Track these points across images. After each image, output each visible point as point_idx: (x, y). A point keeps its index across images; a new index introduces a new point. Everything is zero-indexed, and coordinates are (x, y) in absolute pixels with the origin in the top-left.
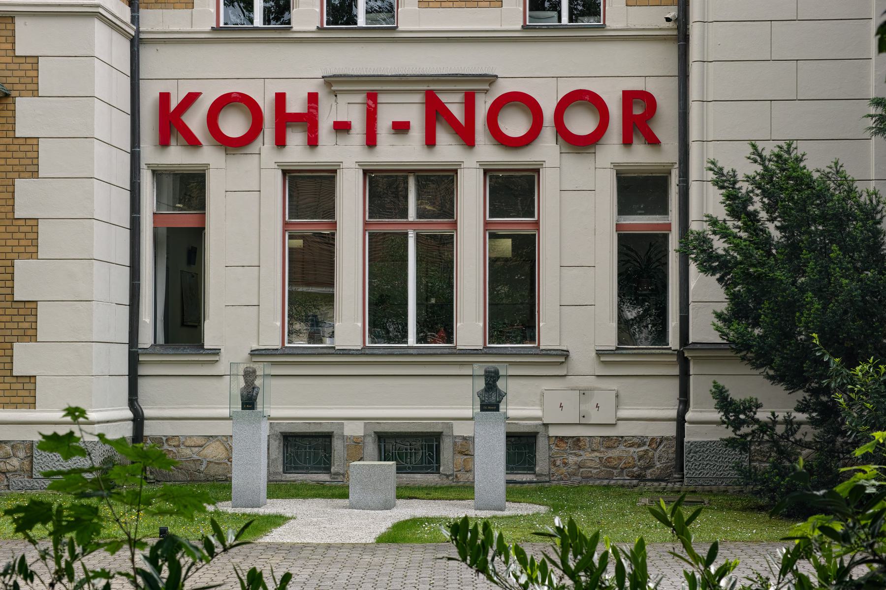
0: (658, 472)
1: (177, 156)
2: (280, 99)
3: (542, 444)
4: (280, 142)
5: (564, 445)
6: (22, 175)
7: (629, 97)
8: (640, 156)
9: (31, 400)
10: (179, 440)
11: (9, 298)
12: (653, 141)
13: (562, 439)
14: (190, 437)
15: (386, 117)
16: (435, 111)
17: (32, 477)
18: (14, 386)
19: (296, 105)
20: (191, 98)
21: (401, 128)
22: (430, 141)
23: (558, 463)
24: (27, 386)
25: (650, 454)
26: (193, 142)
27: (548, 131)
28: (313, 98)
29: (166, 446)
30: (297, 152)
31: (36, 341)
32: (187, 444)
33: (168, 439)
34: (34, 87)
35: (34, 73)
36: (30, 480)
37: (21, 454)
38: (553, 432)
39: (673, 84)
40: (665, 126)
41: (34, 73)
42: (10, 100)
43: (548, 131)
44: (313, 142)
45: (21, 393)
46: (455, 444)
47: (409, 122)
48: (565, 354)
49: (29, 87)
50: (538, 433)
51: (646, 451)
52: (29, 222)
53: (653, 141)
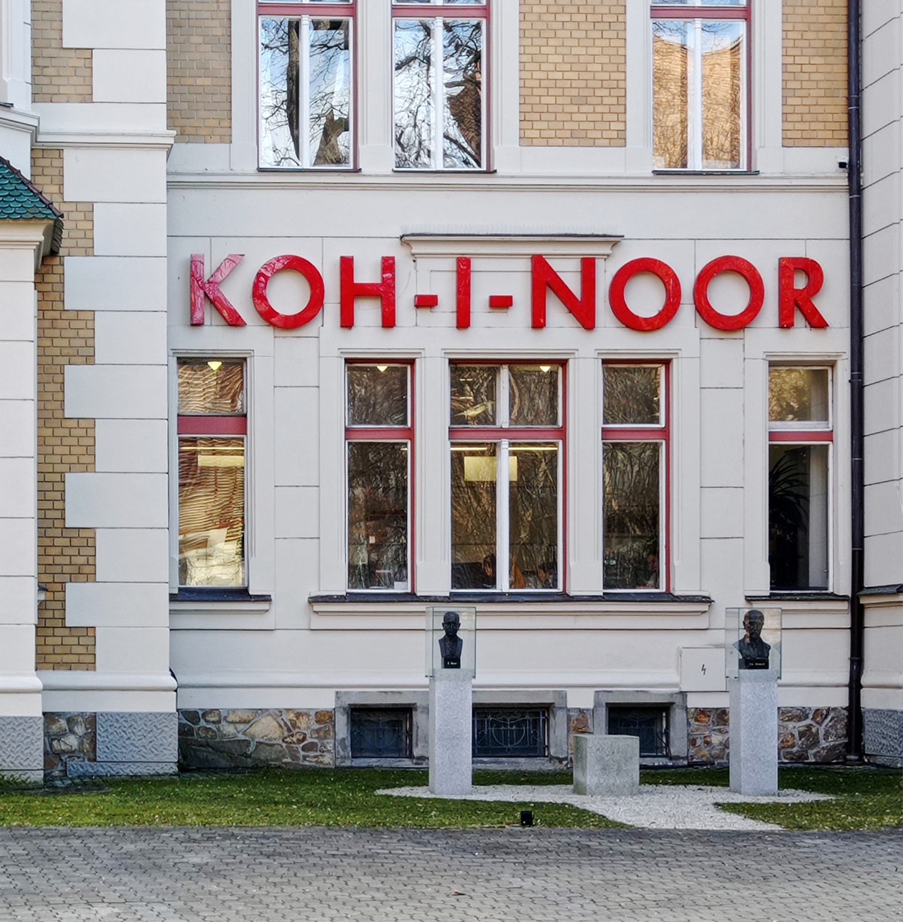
0: (824, 753)
1: (214, 338)
2: (347, 265)
3: (678, 717)
4: (347, 321)
5: (706, 719)
6: (73, 360)
7: (789, 267)
8: (803, 342)
9: (89, 659)
10: (219, 714)
11: (58, 524)
12: (817, 322)
13: (703, 712)
14: (234, 711)
15: (482, 291)
16: (544, 280)
17: (95, 760)
18: (67, 641)
19: (367, 273)
20: (234, 261)
21: (501, 303)
22: (538, 321)
23: (699, 742)
24: (83, 641)
25: (814, 730)
26: (234, 321)
27: (687, 310)
28: (388, 265)
29: (203, 723)
30: (368, 336)
31: (95, 581)
32: (230, 719)
33: (206, 713)
34: (88, 243)
35: (87, 225)
36: (92, 764)
37: (80, 730)
38: (693, 702)
39: (843, 250)
40: (833, 302)
41: (87, 225)
42: (57, 261)
43: (687, 310)
44: (389, 321)
45: (76, 649)
46: (569, 719)
47: (436, 296)
48: (707, 600)
49: (82, 243)
50: (674, 703)
51: (809, 727)
52: (83, 424)
53: (817, 322)
